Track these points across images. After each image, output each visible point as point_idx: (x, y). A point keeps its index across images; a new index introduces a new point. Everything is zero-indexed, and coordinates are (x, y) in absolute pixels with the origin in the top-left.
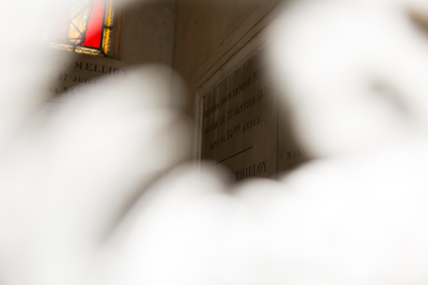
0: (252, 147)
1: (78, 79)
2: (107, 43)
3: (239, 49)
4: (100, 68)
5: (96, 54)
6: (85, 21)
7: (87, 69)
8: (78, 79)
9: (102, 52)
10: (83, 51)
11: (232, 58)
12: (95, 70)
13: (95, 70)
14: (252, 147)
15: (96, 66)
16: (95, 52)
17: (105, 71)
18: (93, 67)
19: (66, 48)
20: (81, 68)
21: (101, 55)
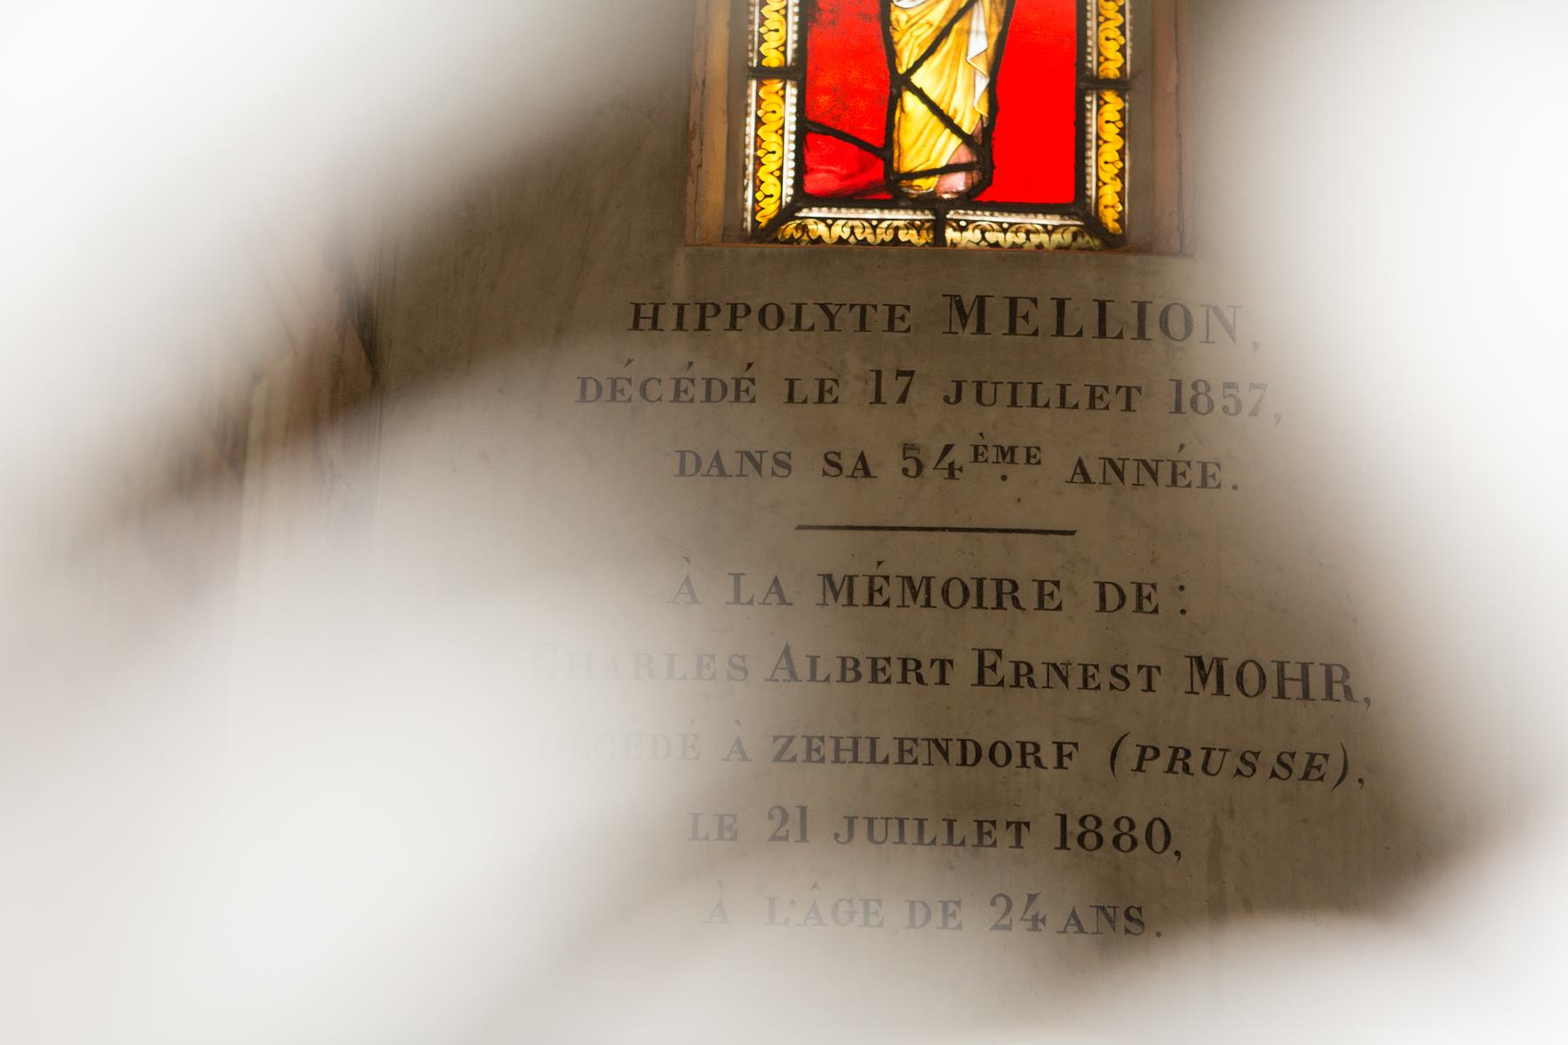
0: (1075, 532)
1: (969, 391)
2: (1108, 173)
3: (994, 171)
4: (1082, 315)
5: (1057, 237)
6: (982, 67)
7: (1012, 330)
8: (969, 391)
9: (1092, 224)
10: (983, 232)
11: (1101, 197)
12: (1102, 333)
13: (1060, 331)
14: (1075, 532)
15: (1061, 304)
16: (1049, 231)
17: (1112, 328)
18: (1045, 316)
19: (897, 229)
20: (980, 329)
21: (1085, 240)
